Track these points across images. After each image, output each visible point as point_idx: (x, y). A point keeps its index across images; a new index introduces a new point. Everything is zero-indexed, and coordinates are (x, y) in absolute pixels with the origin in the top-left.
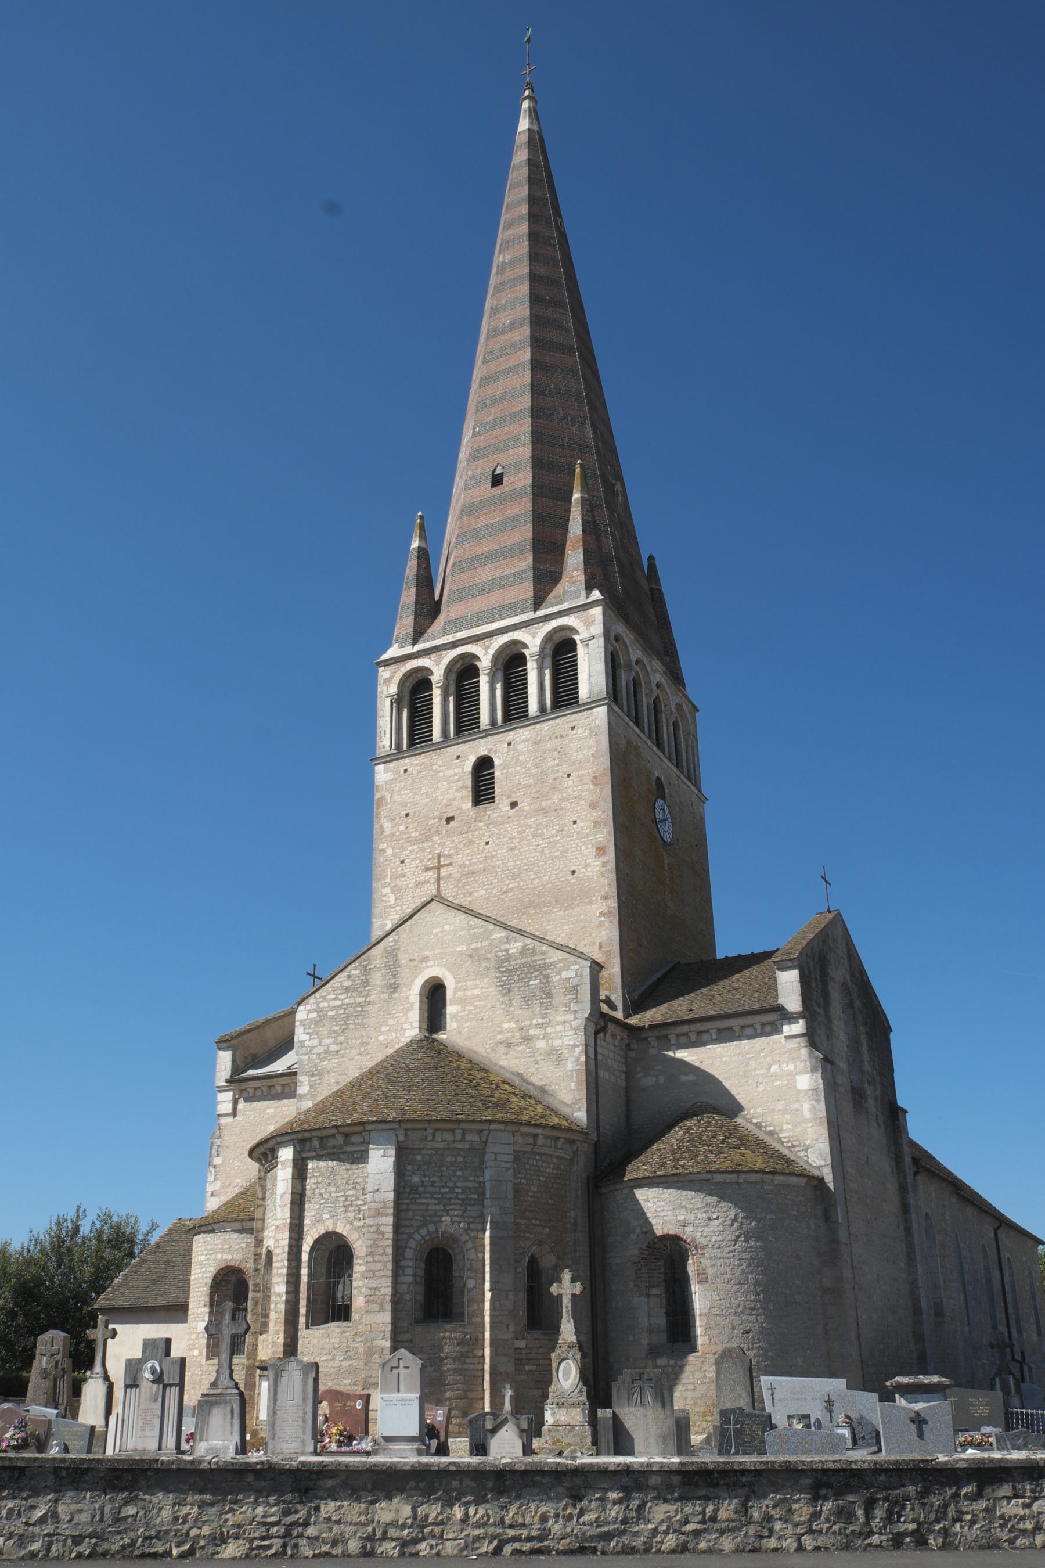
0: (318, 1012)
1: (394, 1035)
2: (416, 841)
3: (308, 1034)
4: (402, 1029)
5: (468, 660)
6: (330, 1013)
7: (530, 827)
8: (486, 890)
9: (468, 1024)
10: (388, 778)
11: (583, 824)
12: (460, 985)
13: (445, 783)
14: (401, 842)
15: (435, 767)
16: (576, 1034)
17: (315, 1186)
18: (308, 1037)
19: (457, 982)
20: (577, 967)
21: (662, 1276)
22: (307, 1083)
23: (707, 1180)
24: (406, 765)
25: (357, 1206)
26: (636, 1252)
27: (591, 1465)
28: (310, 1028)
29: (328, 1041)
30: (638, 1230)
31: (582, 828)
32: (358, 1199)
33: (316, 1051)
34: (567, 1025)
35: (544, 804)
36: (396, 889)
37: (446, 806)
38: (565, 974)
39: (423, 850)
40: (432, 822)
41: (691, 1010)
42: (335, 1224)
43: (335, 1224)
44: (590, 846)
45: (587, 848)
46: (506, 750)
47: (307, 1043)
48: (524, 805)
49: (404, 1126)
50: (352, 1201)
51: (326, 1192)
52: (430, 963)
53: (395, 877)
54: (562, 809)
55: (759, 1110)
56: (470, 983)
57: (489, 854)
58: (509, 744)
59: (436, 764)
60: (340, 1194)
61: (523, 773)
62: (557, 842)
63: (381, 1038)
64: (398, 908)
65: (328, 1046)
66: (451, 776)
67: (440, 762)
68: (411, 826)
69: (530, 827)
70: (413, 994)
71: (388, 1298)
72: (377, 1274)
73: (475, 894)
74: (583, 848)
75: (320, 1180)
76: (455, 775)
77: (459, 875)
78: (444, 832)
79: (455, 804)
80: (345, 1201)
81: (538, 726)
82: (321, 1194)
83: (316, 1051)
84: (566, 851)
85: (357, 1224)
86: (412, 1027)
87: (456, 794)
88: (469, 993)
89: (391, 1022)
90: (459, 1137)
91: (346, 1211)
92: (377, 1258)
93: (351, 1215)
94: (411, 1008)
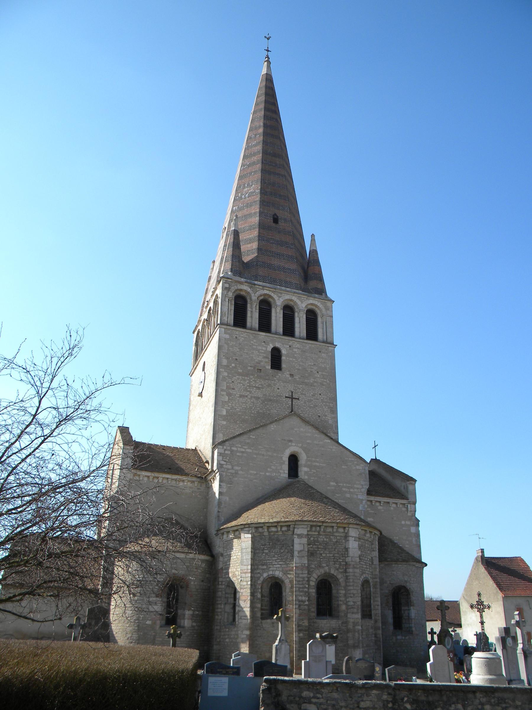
0: (231, 452)
1: (275, 474)
2: (239, 374)
3: (225, 461)
4: (279, 472)
5: (267, 297)
6: (238, 454)
7: (299, 389)
8: (277, 411)
9: (313, 478)
10: (226, 337)
11: (324, 397)
12: (309, 459)
13: (257, 352)
14: (233, 372)
15: (252, 342)
16: (363, 495)
17: (316, 549)
18: (225, 463)
19: (308, 457)
20: (363, 465)
21: (114, 582)
22: (225, 487)
23: (414, 565)
24: (236, 334)
25: (340, 562)
26: (387, 591)
27: (439, 686)
28: (226, 458)
29: (237, 468)
30: (388, 582)
31: (323, 398)
32: (340, 559)
33: (230, 471)
34: (359, 490)
35: (306, 381)
36: (229, 395)
37: (257, 363)
38: (358, 467)
39: (245, 380)
40: (249, 368)
41: (170, 469)
42: (330, 569)
43: (330, 569)
44: (327, 407)
45: (325, 408)
46: (288, 349)
47: (224, 466)
48: (297, 377)
49: (324, 524)
50: (337, 559)
51: (324, 553)
52: (293, 444)
53: (228, 387)
54: (314, 386)
55: (397, 538)
56: (313, 459)
57: (279, 394)
58: (290, 346)
59: (253, 341)
60: (331, 555)
61: (296, 363)
62: (312, 400)
63: (267, 474)
64: (230, 404)
65: (237, 470)
66: (261, 350)
67: (255, 341)
68: (238, 366)
69: (299, 389)
70: (286, 459)
71: (360, 607)
72: (356, 595)
73: (272, 411)
74: (324, 407)
75: (319, 547)
76: (262, 350)
77: (263, 399)
78: (256, 375)
79: (262, 364)
80: (334, 559)
81: (304, 344)
82: (321, 554)
83: (230, 471)
84: (316, 406)
85: (340, 570)
86: (284, 473)
87: (263, 359)
88: (314, 464)
89: (273, 467)
90: (335, 530)
91: (334, 564)
92: (355, 588)
93: (337, 566)
94: (284, 463)
